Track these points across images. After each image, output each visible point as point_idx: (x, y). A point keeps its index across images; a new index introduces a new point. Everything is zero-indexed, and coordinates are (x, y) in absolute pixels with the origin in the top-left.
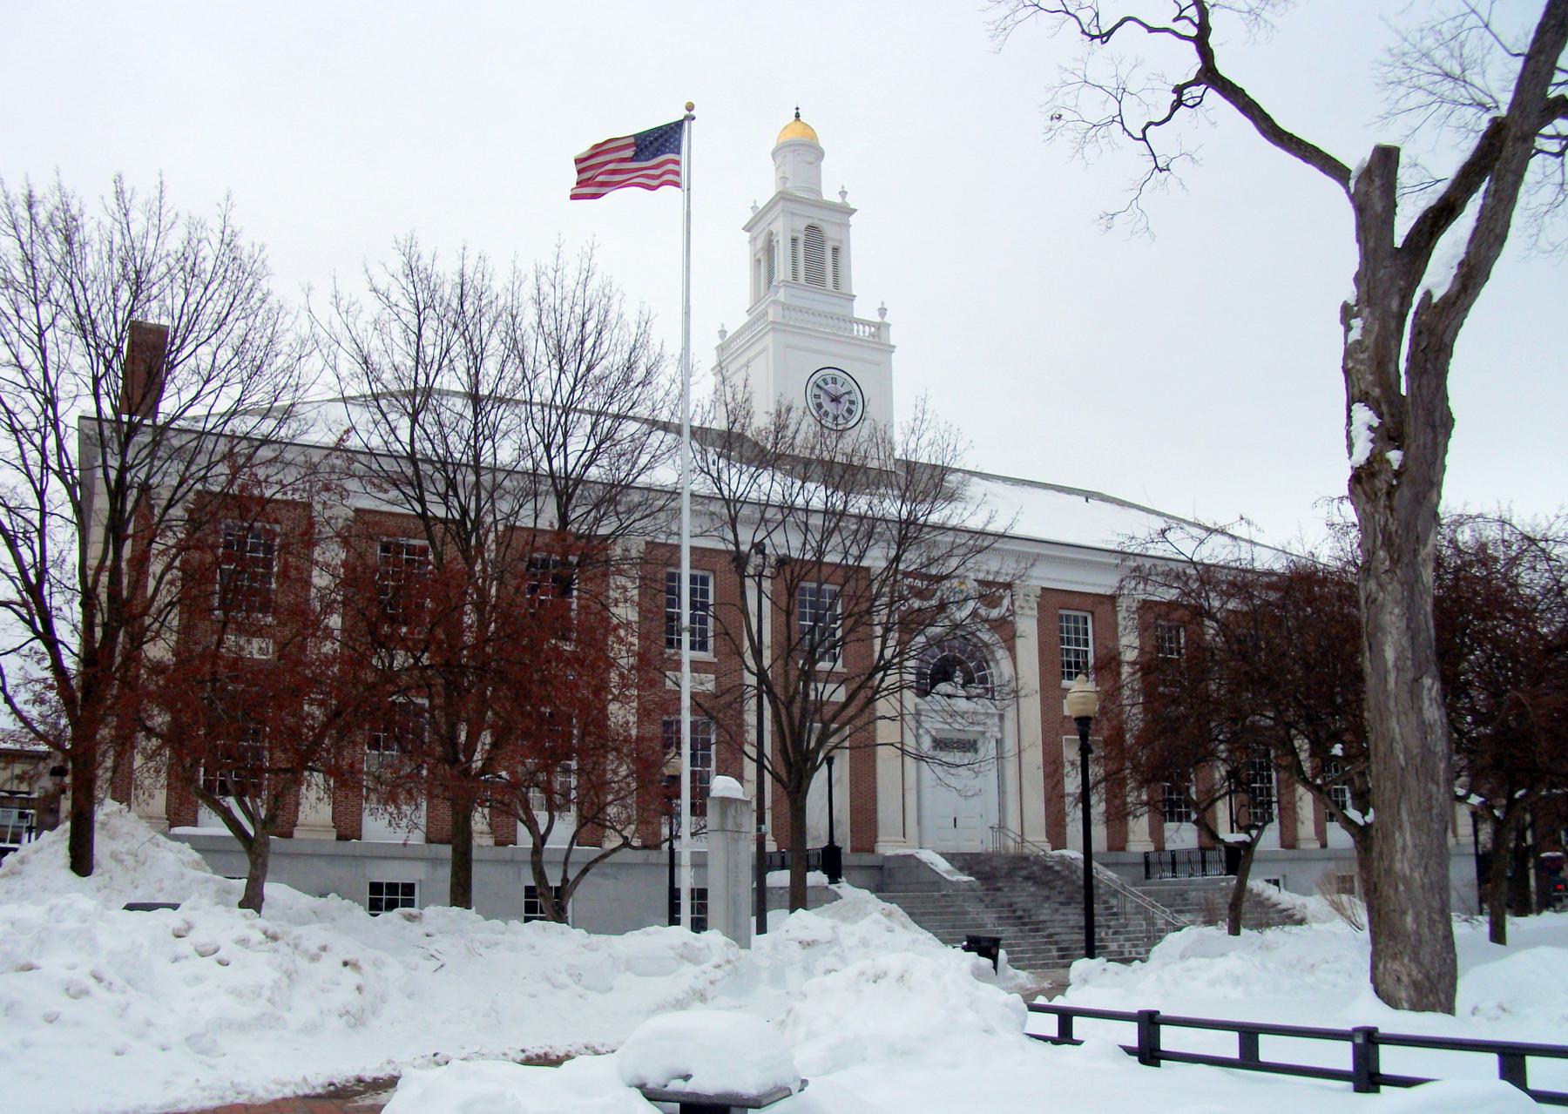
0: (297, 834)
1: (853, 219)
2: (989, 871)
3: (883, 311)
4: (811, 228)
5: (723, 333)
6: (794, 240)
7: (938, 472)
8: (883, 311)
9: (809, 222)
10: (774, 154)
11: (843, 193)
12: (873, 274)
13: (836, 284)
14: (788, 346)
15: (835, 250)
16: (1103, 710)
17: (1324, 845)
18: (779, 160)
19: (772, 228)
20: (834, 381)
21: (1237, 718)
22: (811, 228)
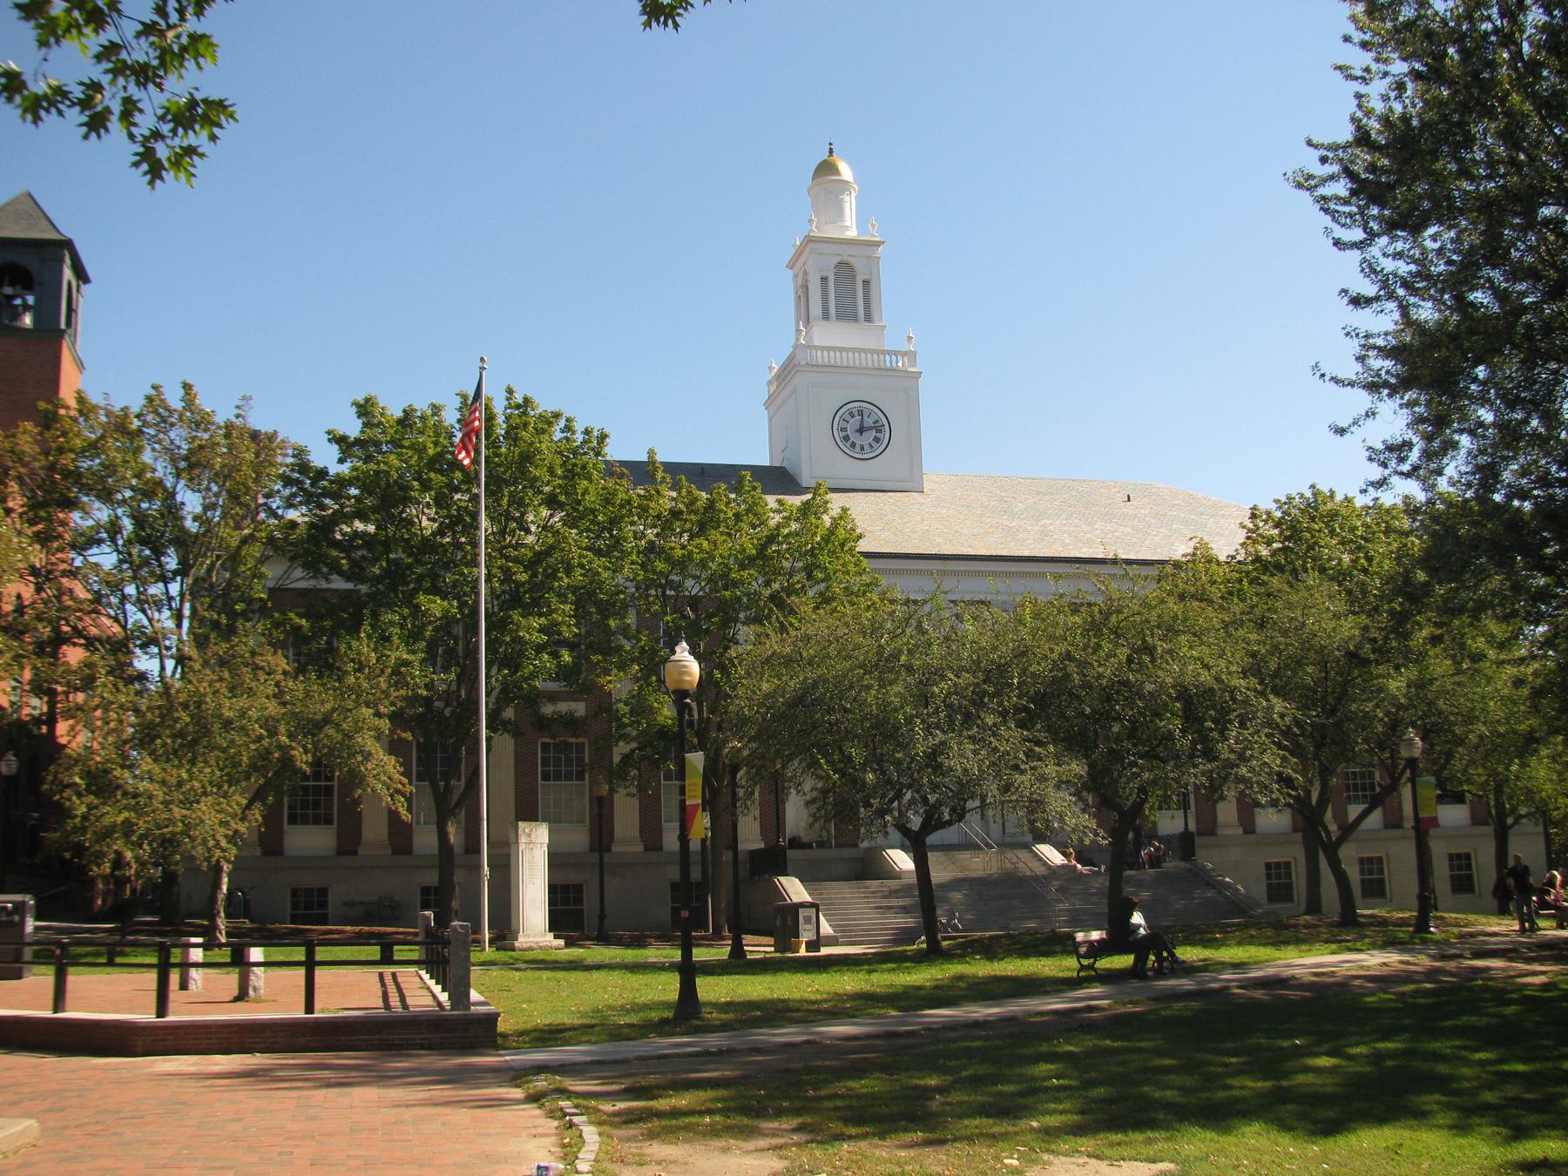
0: (361, 852)
6: (824, 279)
15: (866, 283)
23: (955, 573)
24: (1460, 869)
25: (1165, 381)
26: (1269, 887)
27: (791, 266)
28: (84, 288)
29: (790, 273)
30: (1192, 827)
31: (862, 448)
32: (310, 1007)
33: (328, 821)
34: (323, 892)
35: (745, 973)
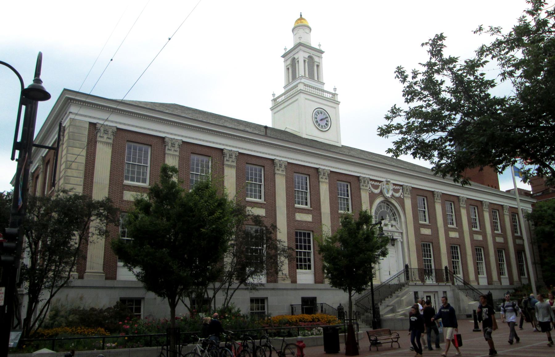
1: (323, 55)
2: (518, 169)
5: (274, 95)
6: (305, 61)
8: (335, 89)
9: (309, 55)
11: (320, 45)
12: (331, 76)
14: (306, 99)
15: (318, 66)
16: (270, 323)
17: (478, 284)
18: (295, 33)
19: (296, 56)
22: (310, 57)
33: (309, 268)
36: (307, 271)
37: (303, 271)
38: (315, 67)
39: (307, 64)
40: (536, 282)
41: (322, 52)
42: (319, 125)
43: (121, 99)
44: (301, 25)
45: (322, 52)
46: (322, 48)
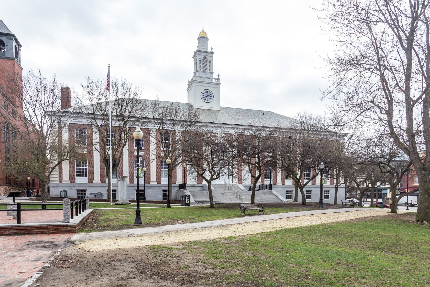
0: (94, 183)
1: (214, 55)
3: (219, 76)
4: (204, 57)
6: (200, 61)
7: (120, 101)
8: (219, 76)
10: (198, 39)
13: (210, 70)
15: (210, 62)
20: (210, 98)
21: (370, 177)
22: (205, 57)
23: (225, 127)
24: (308, 193)
25: (287, 53)
26: (163, 196)
27: (193, 58)
28: (21, 48)
29: (193, 59)
30: (272, 183)
31: (205, 99)
32: (19, 222)
33: (86, 176)
34: (85, 191)
35: (55, 234)
36: (85, 177)
37: (79, 177)
38: (208, 63)
39: (202, 62)
40: (99, 210)
41: (213, 53)
42: (205, 99)
43: (71, 96)
44: (203, 38)
45: (213, 53)
46: (213, 51)
